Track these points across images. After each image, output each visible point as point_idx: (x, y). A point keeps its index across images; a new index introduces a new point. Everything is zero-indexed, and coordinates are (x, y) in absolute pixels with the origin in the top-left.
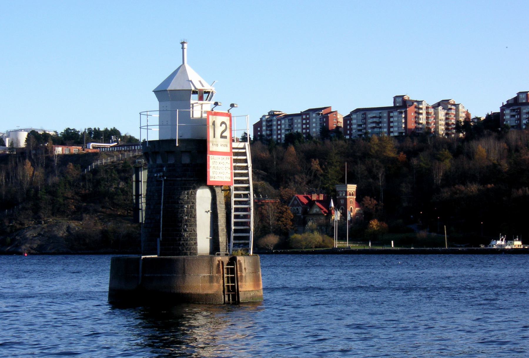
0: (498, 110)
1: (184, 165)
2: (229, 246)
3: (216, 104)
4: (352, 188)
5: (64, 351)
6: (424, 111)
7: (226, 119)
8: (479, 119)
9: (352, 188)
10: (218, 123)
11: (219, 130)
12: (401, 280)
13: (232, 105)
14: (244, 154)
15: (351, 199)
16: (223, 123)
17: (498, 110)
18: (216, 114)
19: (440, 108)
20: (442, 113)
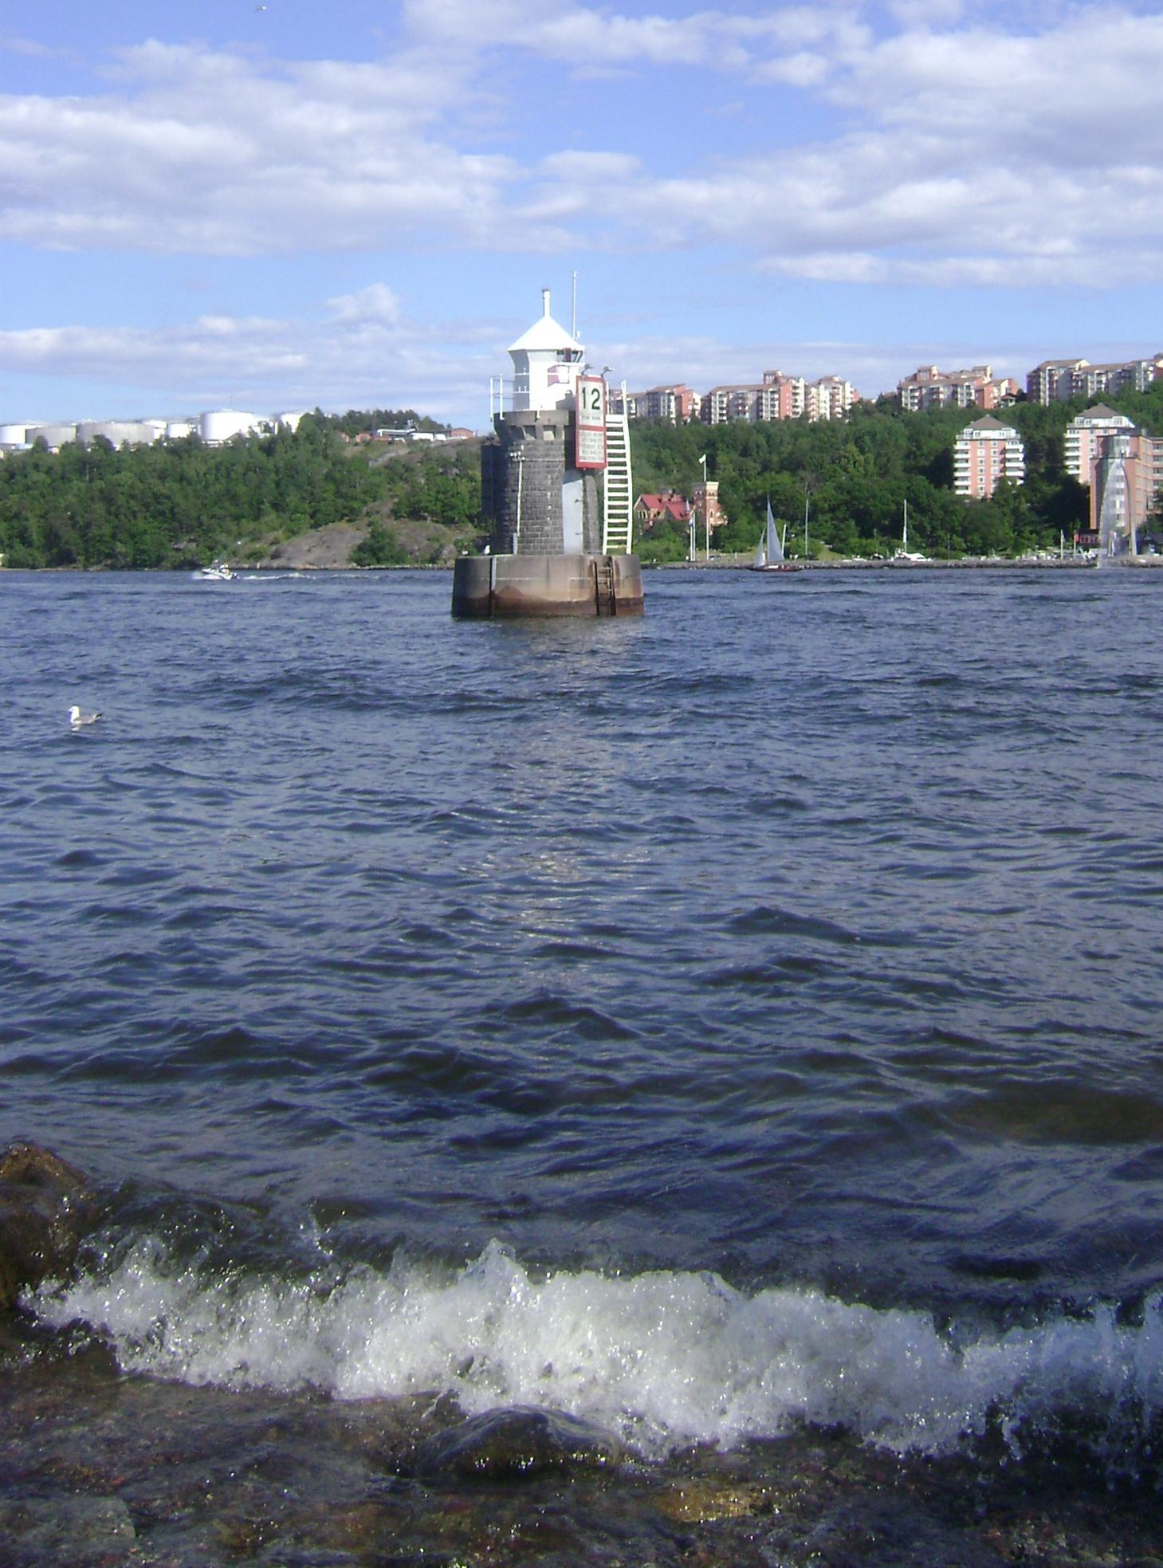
0: (896, 391)
1: (547, 443)
2: (935, 577)
3: (587, 367)
4: (712, 487)
5: (949, 864)
6: (801, 391)
7: (598, 386)
8: (869, 402)
9: (712, 487)
10: (589, 390)
11: (590, 399)
12: (426, 595)
13: (607, 369)
14: (621, 430)
15: (712, 501)
16: (595, 390)
17: (896, 391)
18: (587, 379)
19: (822, 387)
20: (824, 394)
